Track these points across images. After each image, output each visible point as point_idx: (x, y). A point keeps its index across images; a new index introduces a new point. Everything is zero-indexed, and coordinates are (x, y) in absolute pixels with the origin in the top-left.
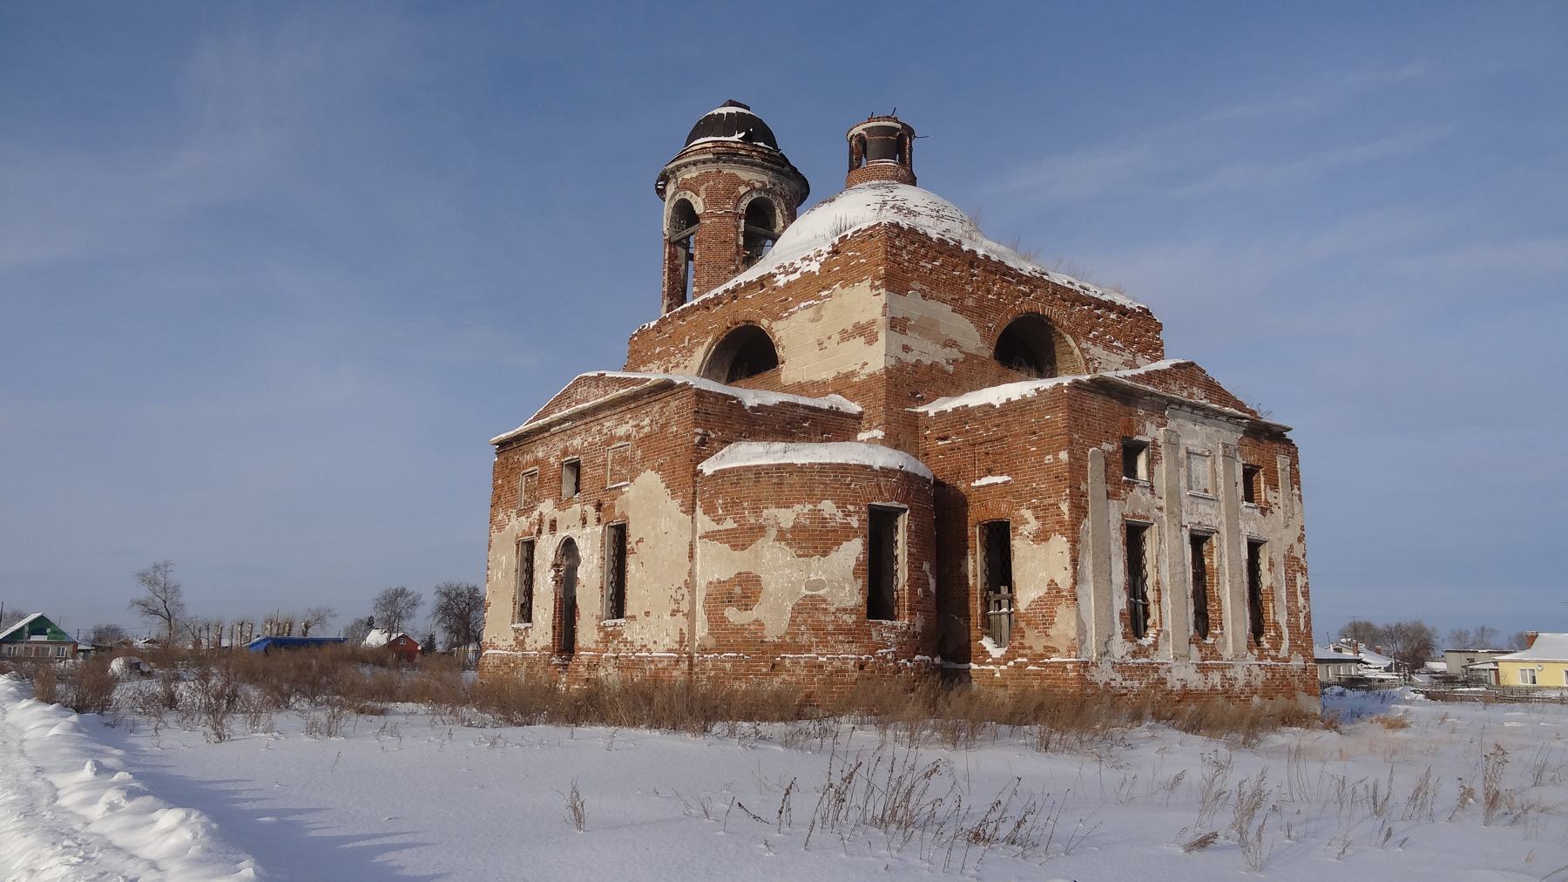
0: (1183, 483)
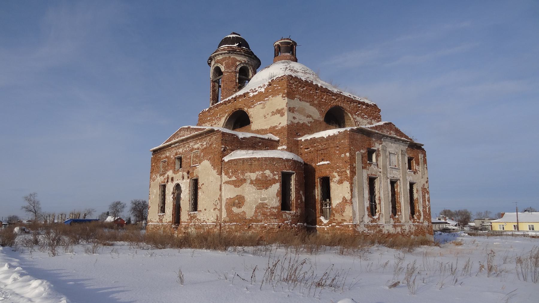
0: (388, 163)
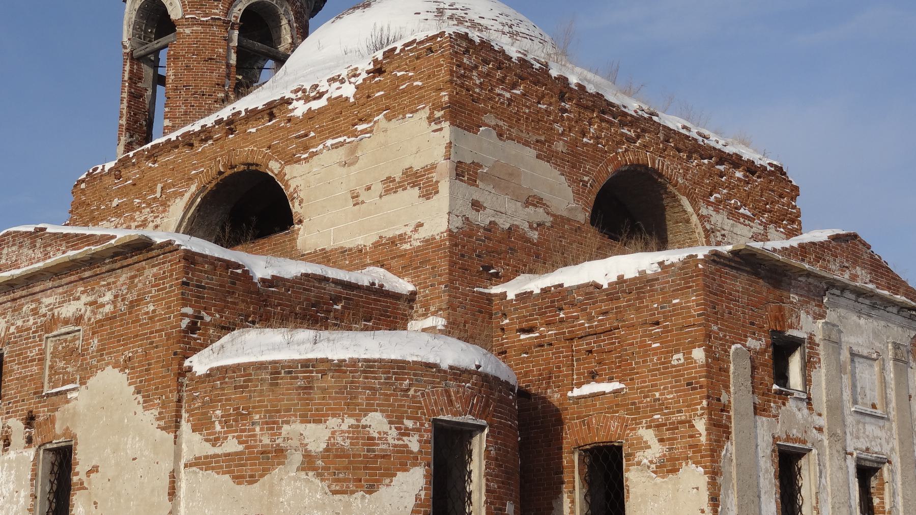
0: (847, 395)
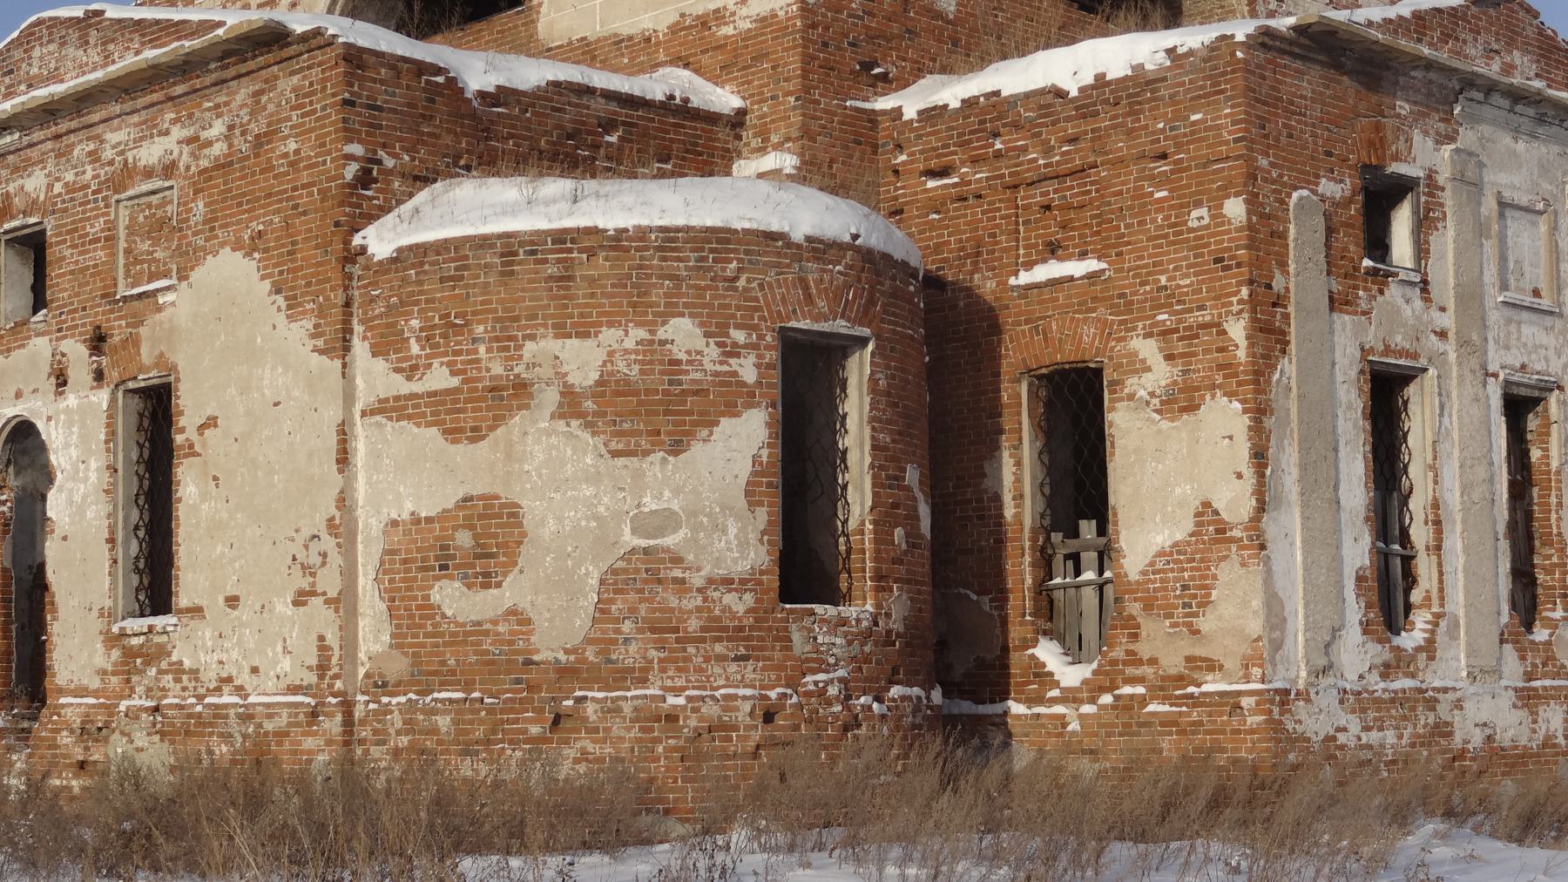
0: (1490, 275)
